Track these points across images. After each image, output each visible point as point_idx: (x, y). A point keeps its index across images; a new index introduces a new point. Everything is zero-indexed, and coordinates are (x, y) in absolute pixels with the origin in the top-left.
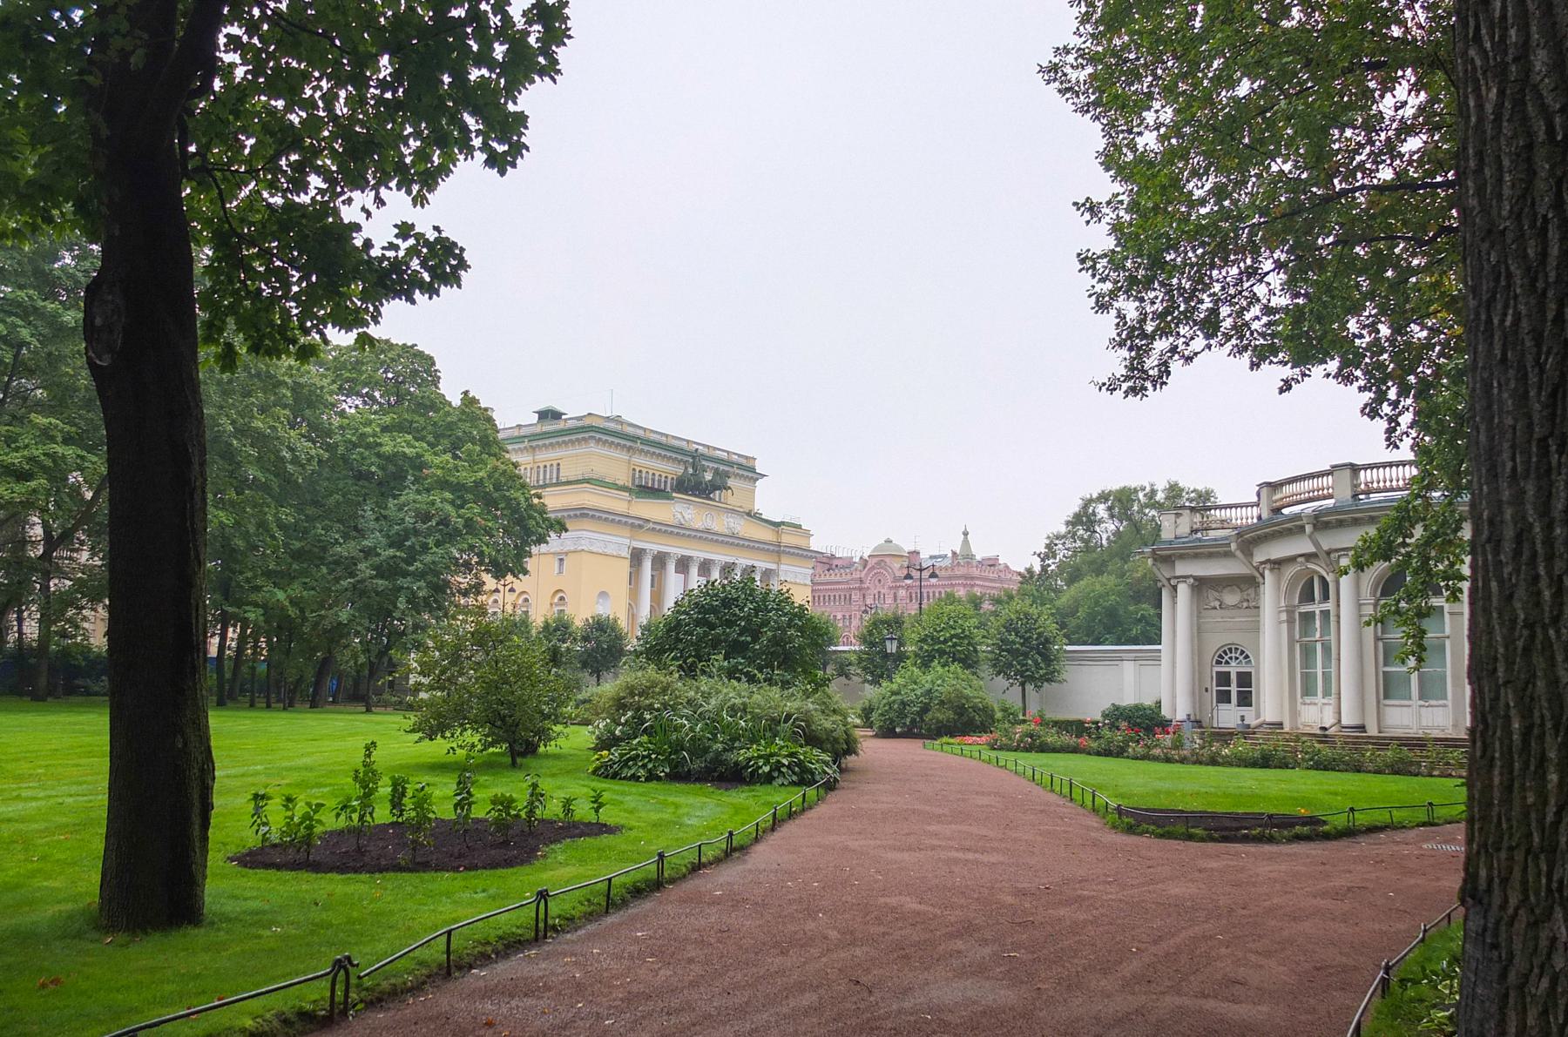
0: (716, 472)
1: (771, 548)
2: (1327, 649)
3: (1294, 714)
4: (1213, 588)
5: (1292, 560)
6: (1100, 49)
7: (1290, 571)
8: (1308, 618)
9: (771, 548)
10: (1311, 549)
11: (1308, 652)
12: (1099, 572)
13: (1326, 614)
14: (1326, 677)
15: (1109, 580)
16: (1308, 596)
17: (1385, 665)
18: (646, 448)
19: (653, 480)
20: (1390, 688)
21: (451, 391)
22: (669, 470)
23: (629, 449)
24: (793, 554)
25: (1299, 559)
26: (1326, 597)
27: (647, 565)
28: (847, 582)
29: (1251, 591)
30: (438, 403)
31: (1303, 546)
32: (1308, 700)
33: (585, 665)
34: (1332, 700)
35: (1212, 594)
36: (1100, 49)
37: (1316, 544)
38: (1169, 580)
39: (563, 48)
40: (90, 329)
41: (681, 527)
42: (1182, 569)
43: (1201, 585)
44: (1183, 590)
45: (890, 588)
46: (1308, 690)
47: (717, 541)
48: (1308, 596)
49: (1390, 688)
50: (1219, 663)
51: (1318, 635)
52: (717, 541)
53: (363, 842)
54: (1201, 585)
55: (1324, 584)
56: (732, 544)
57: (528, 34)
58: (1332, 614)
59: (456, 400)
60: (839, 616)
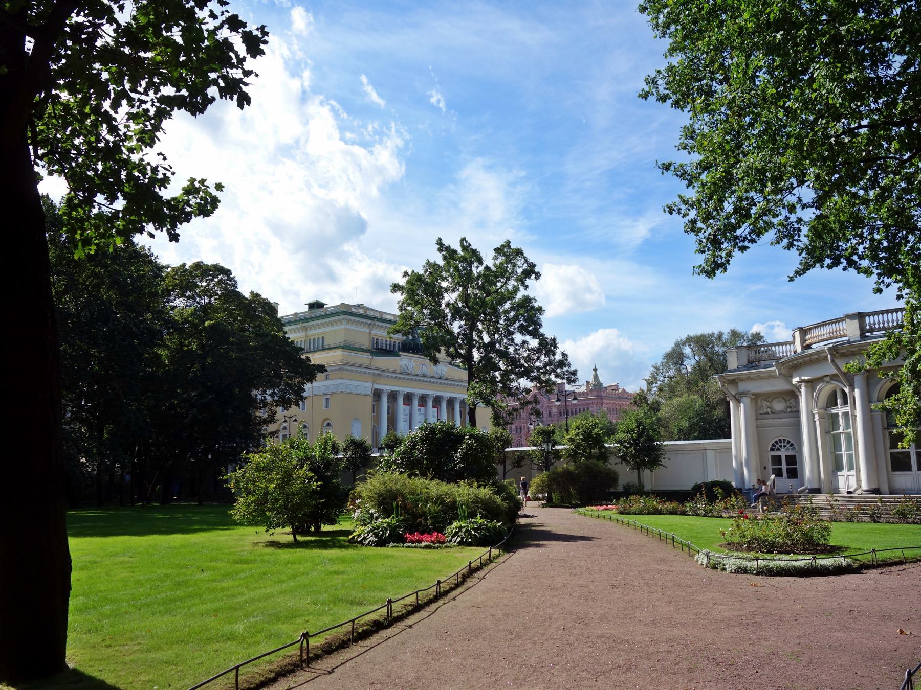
10: (833, 371)
13: (846, 414)
14: (850, 457)
19: (386, 344)
27: (385, 399)
50: (772, 449)
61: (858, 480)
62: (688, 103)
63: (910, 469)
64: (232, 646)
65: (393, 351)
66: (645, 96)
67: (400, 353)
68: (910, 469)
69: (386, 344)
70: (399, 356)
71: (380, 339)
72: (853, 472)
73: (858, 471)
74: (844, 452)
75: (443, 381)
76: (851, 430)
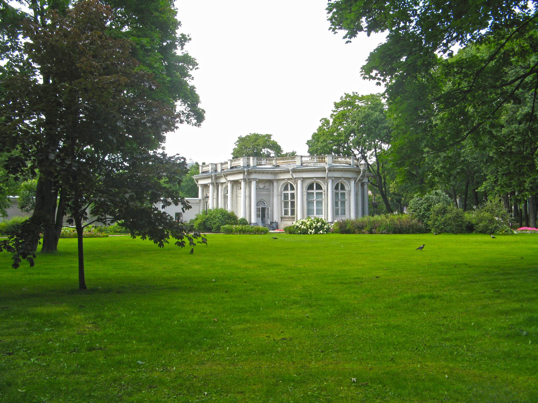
5: (284, 179)
25: (342, 179)
31: (289, 176)
37: (292, 176)
39: (12, 257)
40: (7, 4)
42: (253, 176)
43: (259, 182)
48: (286, 189)
51: (315, 199)
53: (378, 228)
54: (259, 182)
55: (291, 185)
57: (23, 194)
58: (295, 194)
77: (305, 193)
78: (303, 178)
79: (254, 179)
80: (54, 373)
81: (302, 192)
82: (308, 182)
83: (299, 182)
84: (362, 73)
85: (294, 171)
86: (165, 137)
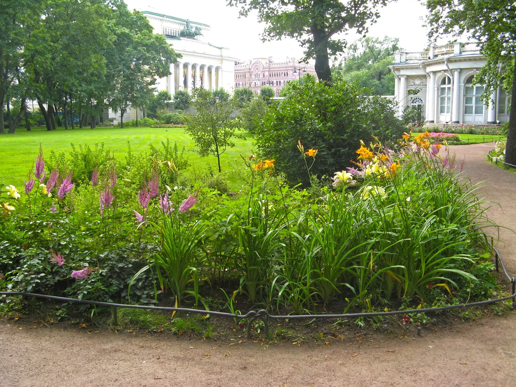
0: (196, 28)
1: (219, 58)
2: (449, 99)
3: (438, 118)
4: (412, 79)
5: (440, 71)
6: (483, 23)
7: (439, 75)
8: (443, 89)
9: (219, 58)
10: (446, 68)
11: (443, 99)
12: (358, 68)
13: (449, 88)
14: (448, 108)
15: (363, 72)
16: (444, 82)
17: (466, 103)
18: (168, 19)
19: (171, 32)
20: (467, 111)
21: (130, 9)
22: (179, 28)
23: (161, 20)
24: (227, 60)
26: (449, 83)
27: (190, 68)
28: (244, 70)
29: (424, 80)
30: (127, 14)
31: (444, 67)
32: (442, 114)
33: (176, 108)
34: (449, 114)
35: (411, 81)
36: (483, 23)
38: (398, 76)
41: (194, 52)
42: (402, 72)
43: (408, 77)
44: (403, 79)
45: (262, 71)
46: (442, 111)
47: (198, 56)
48: (444, 82)
49: (467, 111)
50: (413, 102)
52: (198, 56)
55: (449, 78)
56: (204, 57)
59: (132, 12)
60: (241, 83)
61: (451, 118)
62: (374, 163)
63: (472, 113)
64: (181, 152)
65: (176, 37)
66: (372, 24)
67: (181, 38)
68: (472, 113)
69: (171, 32)
70: (180, 40)
71: (167, 29)
72: (449, 114)
73: (452, 113)
74: (446, 105)
75: (196, 54)
76: (451, 96)
77: (462, 88)
78: (461, 69)
79: (403, 76)
80: (182, 165)
81: (459, 87)
82: (466, 75)
83: (456, 74)
84: (83, 147)
85: (449, 61)
86: (428, 9)
